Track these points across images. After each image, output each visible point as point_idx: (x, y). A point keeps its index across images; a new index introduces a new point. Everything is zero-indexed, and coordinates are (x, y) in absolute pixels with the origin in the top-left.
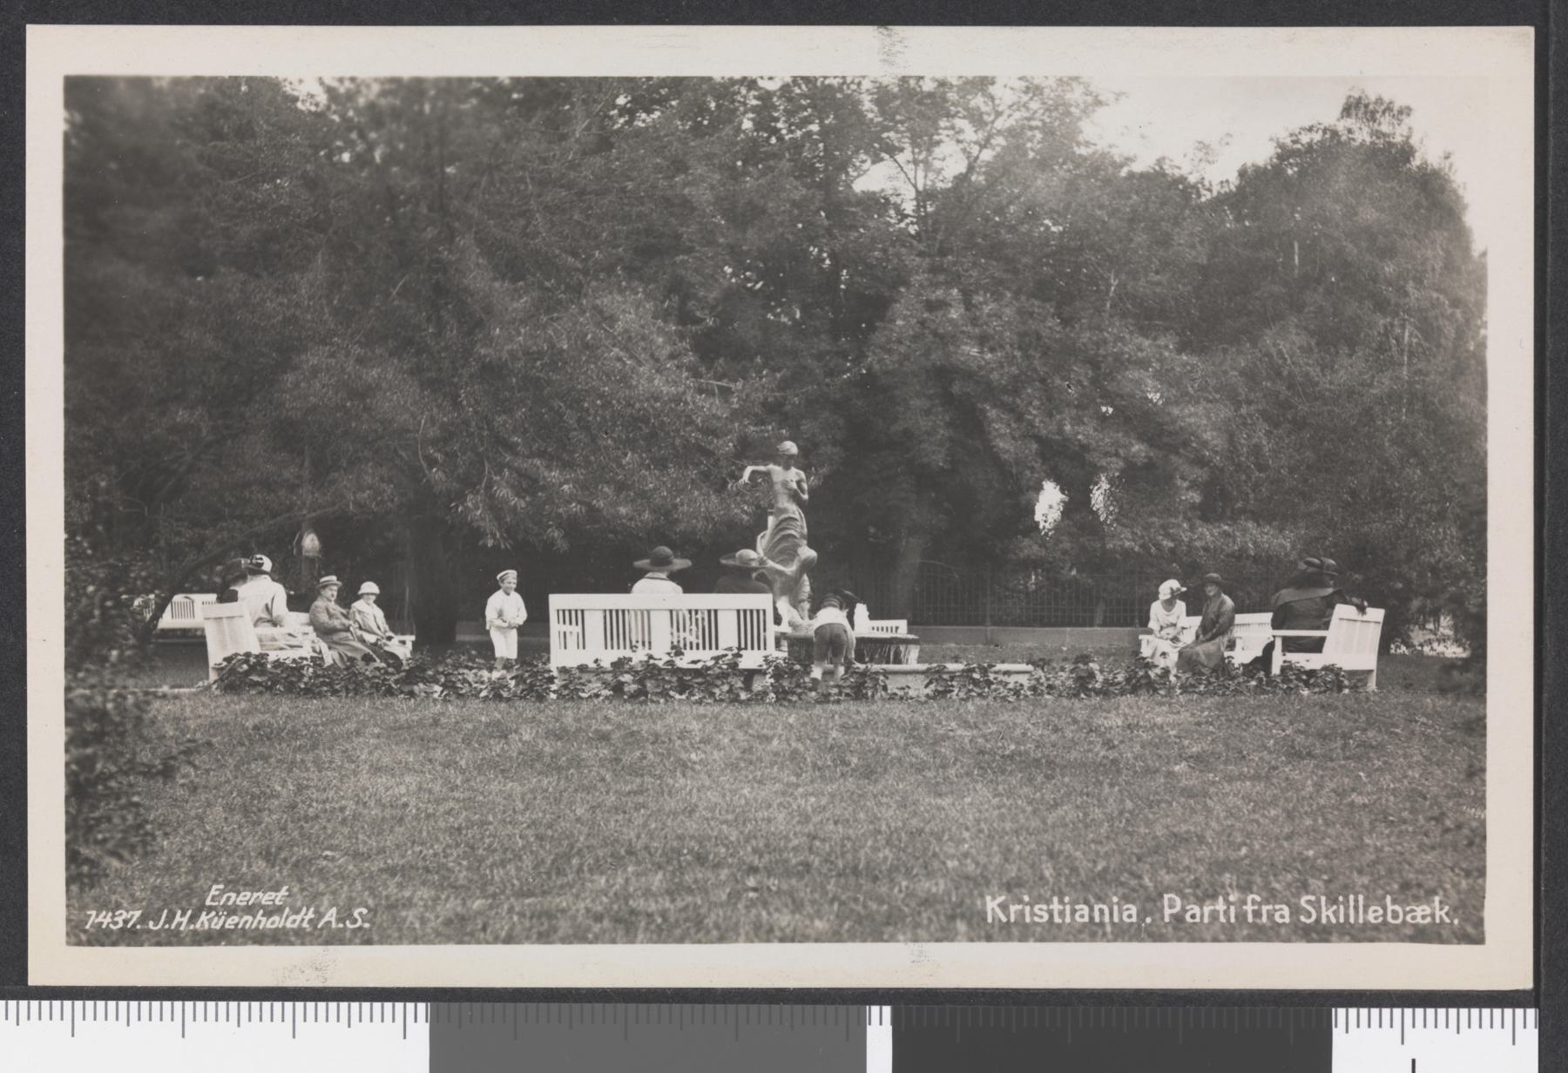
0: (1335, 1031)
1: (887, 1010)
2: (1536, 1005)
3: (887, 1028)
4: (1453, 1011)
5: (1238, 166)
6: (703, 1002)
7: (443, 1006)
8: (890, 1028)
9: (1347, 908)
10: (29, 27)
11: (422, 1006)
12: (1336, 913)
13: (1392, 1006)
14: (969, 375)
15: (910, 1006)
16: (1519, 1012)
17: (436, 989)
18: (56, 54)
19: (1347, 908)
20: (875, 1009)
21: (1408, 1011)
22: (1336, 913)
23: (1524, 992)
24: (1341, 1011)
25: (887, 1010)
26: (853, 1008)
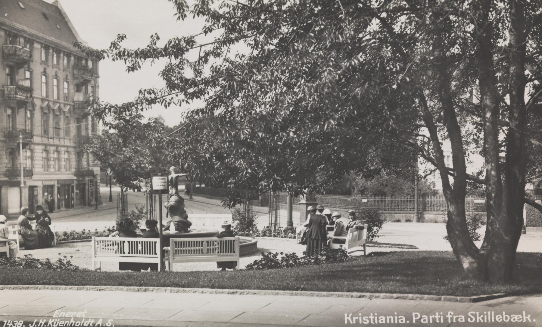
12: (483, 318)
22: (483, 318)
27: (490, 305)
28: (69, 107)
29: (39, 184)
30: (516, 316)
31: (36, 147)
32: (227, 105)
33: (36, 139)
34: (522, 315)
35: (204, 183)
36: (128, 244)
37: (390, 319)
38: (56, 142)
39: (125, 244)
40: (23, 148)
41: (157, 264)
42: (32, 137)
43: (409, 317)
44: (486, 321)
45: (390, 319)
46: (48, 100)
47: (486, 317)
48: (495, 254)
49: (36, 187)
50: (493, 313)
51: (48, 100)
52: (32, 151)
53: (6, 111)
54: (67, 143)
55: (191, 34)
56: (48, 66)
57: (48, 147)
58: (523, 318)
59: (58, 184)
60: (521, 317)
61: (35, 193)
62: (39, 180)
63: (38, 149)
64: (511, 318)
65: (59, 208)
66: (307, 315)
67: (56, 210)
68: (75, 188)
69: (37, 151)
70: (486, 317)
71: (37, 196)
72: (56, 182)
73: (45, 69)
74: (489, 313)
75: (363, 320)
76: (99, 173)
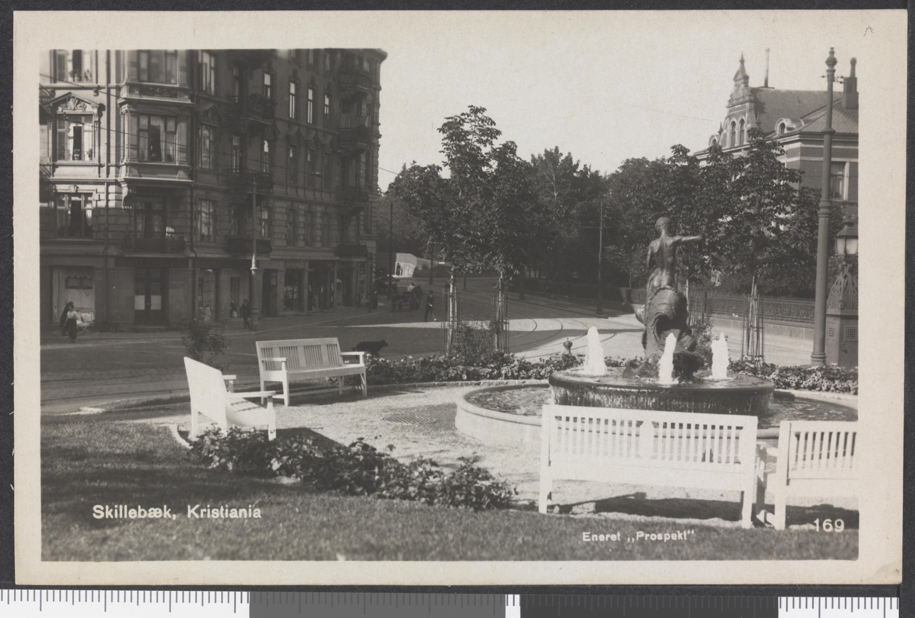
0: (780, 610)
1: (517, 597)
2: (898, 596)
3: (518, 608)
4: (849, 599)
5: (551, 147)
6: (409, 592)
7: (258, 593)
8: (519, 608)
9: (119, 512)
10: (16, 14)
11: (245, 594)
12: (113, 513)
13: (814, 595)
14: (149, 151)
15: (527, 592)
16: (888, 599)
17: (594, 586)
18: (37, 36)
19: (119, 512)
20: (510, 596)
21: (823, 599)
22: (113, 513)
23: (14, 580)
24: (784, 599)
25: (517, 597)
26: (498, 596)
28: (330, 137)
29: (281, 266)
31: (277, 204)
32: (784, 198)
33: (277, 190)
35: (52, 200)
38: (309, 195)
40: (257, 205)
42: (272, 187)
44: (116, 516)
46: (316, 130)
49: (276, 271)
50: (126, 507)
51: (316, 130)
52: (271, 211)
53: (231, 141)
54: (326, 197)
55: (728, 88)
56: (300, 67)
57: (296, 205)
59: (310, 267)
61: (273, 282)
62: (280, 260)
63: (280, 207)
65: (310, 308)
66: (578, 501)
68: (336, 275)
69: (278, 210)
71: (276, 286)
72: (307, 265)
73: (295, 72)
74: (121, 507)
76: (374, 252)
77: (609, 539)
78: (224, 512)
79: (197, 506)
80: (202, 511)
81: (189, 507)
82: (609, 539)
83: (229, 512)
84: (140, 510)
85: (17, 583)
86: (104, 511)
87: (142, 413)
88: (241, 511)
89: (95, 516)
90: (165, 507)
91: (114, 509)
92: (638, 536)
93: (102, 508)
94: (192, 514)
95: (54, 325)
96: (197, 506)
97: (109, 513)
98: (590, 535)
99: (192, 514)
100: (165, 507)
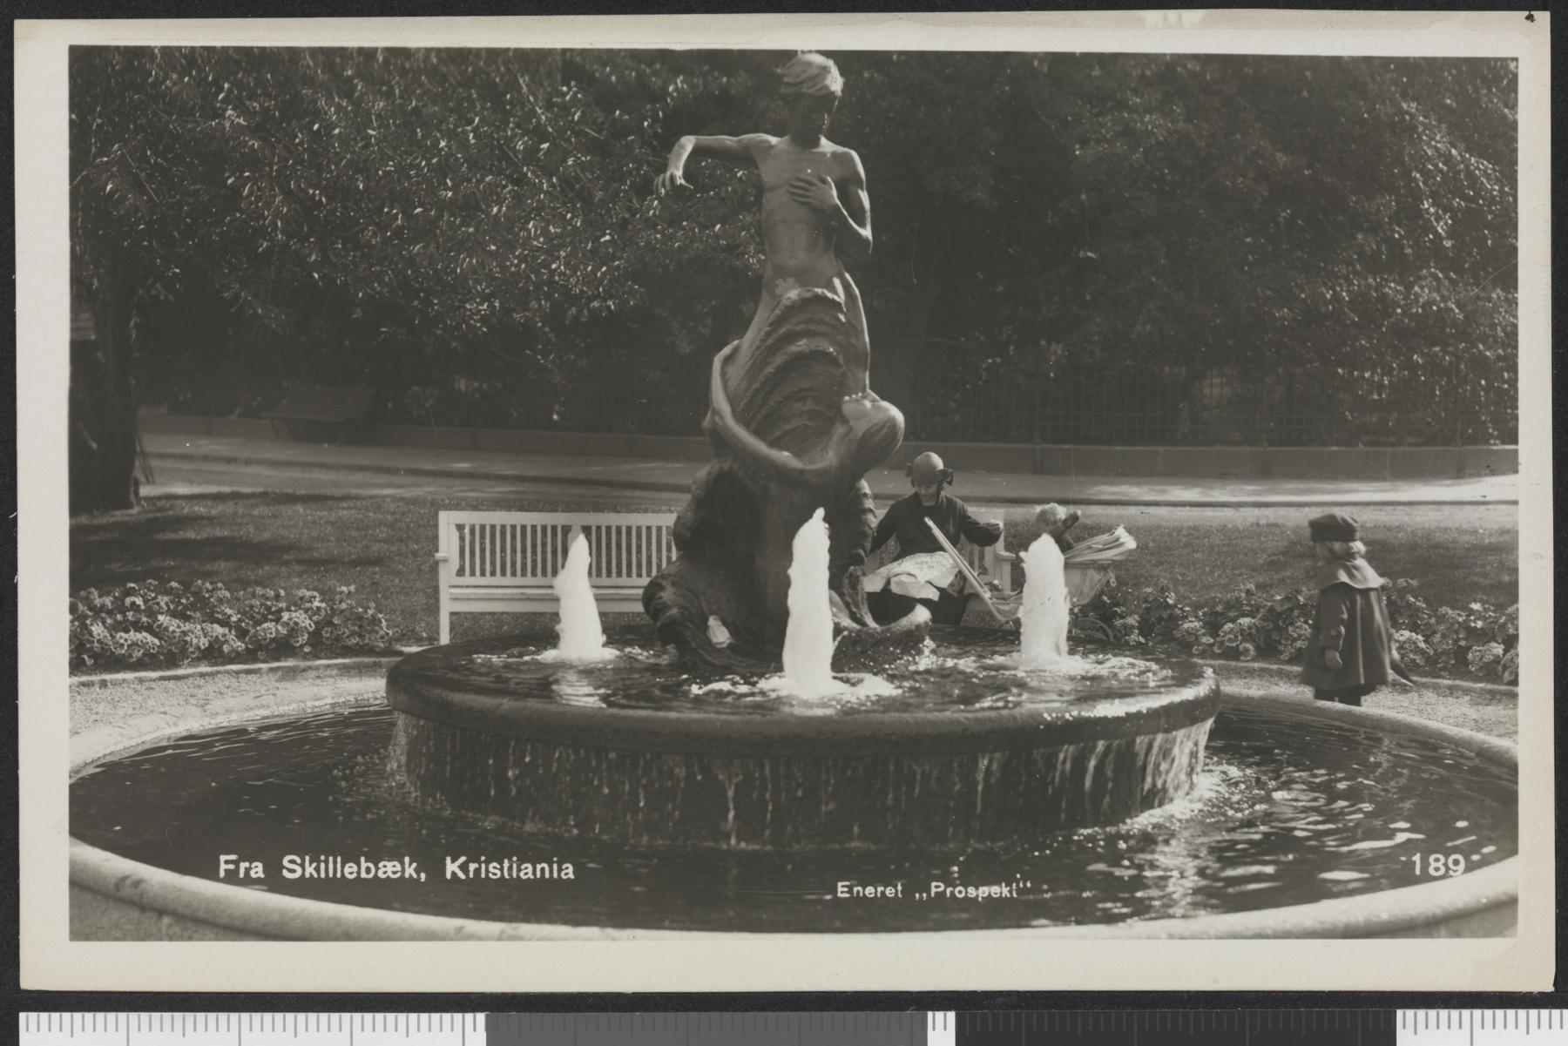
1: (951, 1015)
12: (317, 869)
22: (317, 869)
24: (1399, 1013)
25: (951, 1015)
27: (141, 681)
30: (390, 865)
34: (403, 864)
36: (456, 535)
37: (543, 870)
39: (457, 567)
41: (83, 61)
43: (273, 868)
44: (323, 875)
45: (543, 870)
47: (323, 866)
48: (1081, 254)
58: (403, 870)
60: (399, 868)
64: (377, 869)
67: (554, 592)
70: (323, 866)
75: (487, 871)
77: (883, 893)
78: (510, 868)
79: (463, 859)
80: (472, 866)
81: (448, 860)
82: (883, 893)
83: (519, 870)
84: (364, 865)
85: (26, 984)
86: (302, 865)
87: (165, 743)
88: (539, 867)
89: (285, 873)
90: (407, 859)
91: (319, 862)
92: (934, 890)
93: (298, 860)
94: (454, 873)
95: (1500, 144)
96: (463, 859)
97: (310, 870)
98: (850, 888)
99: (454, 873)
100: (407, 859)
